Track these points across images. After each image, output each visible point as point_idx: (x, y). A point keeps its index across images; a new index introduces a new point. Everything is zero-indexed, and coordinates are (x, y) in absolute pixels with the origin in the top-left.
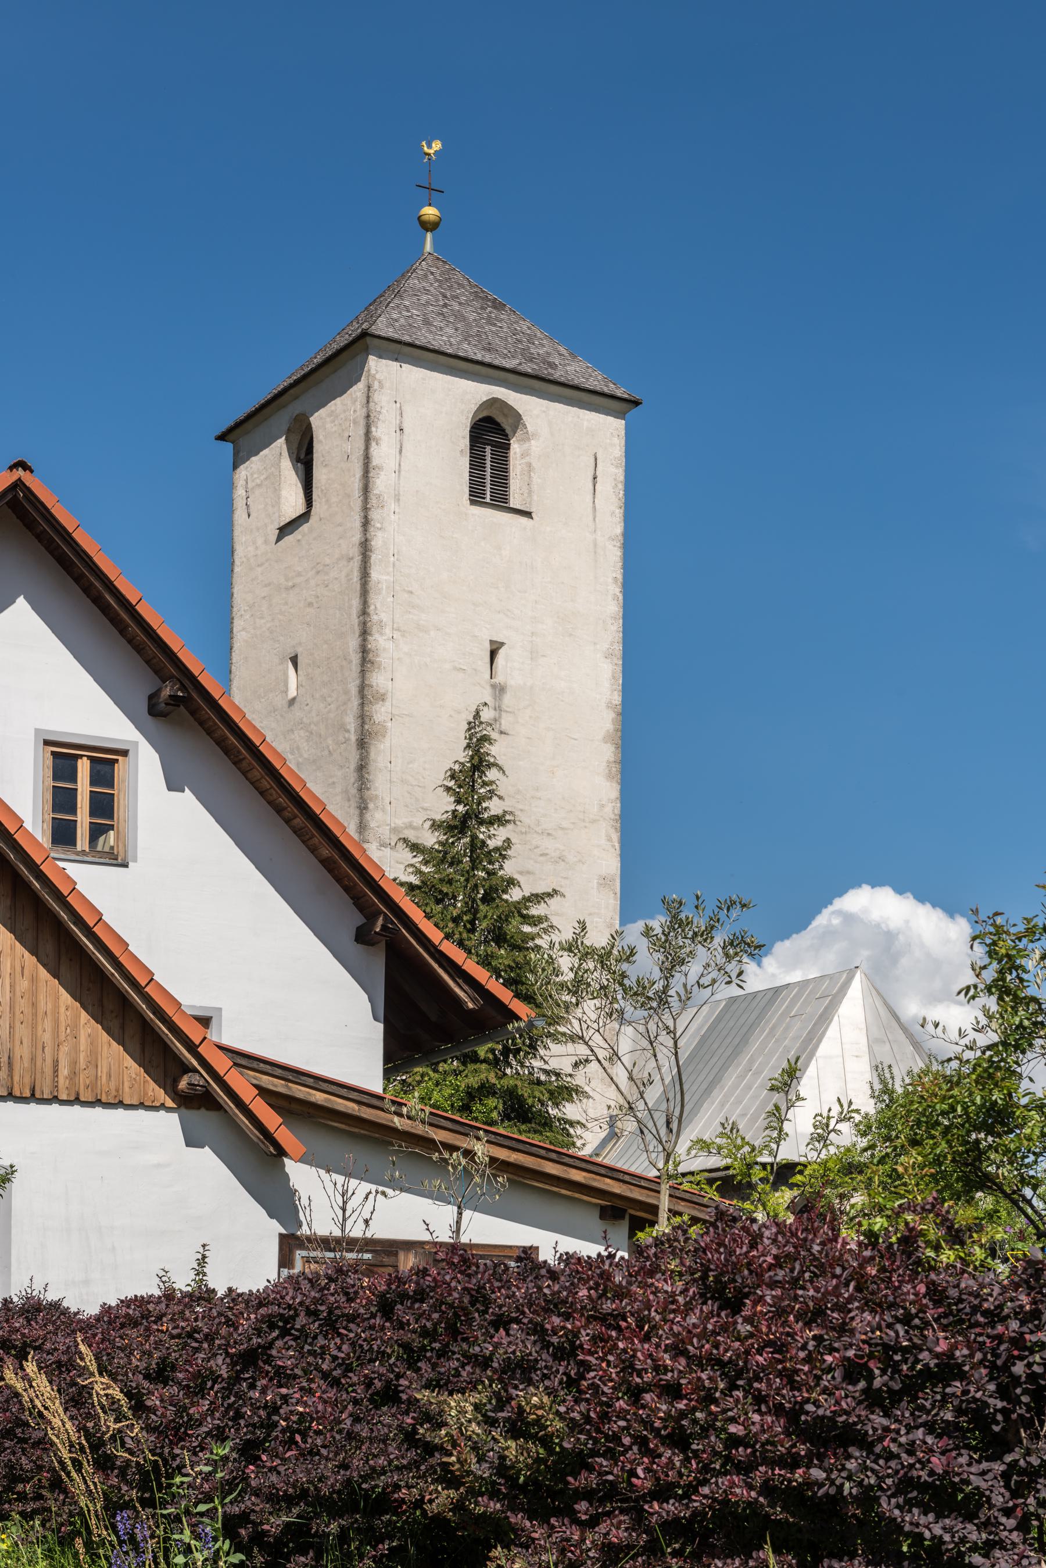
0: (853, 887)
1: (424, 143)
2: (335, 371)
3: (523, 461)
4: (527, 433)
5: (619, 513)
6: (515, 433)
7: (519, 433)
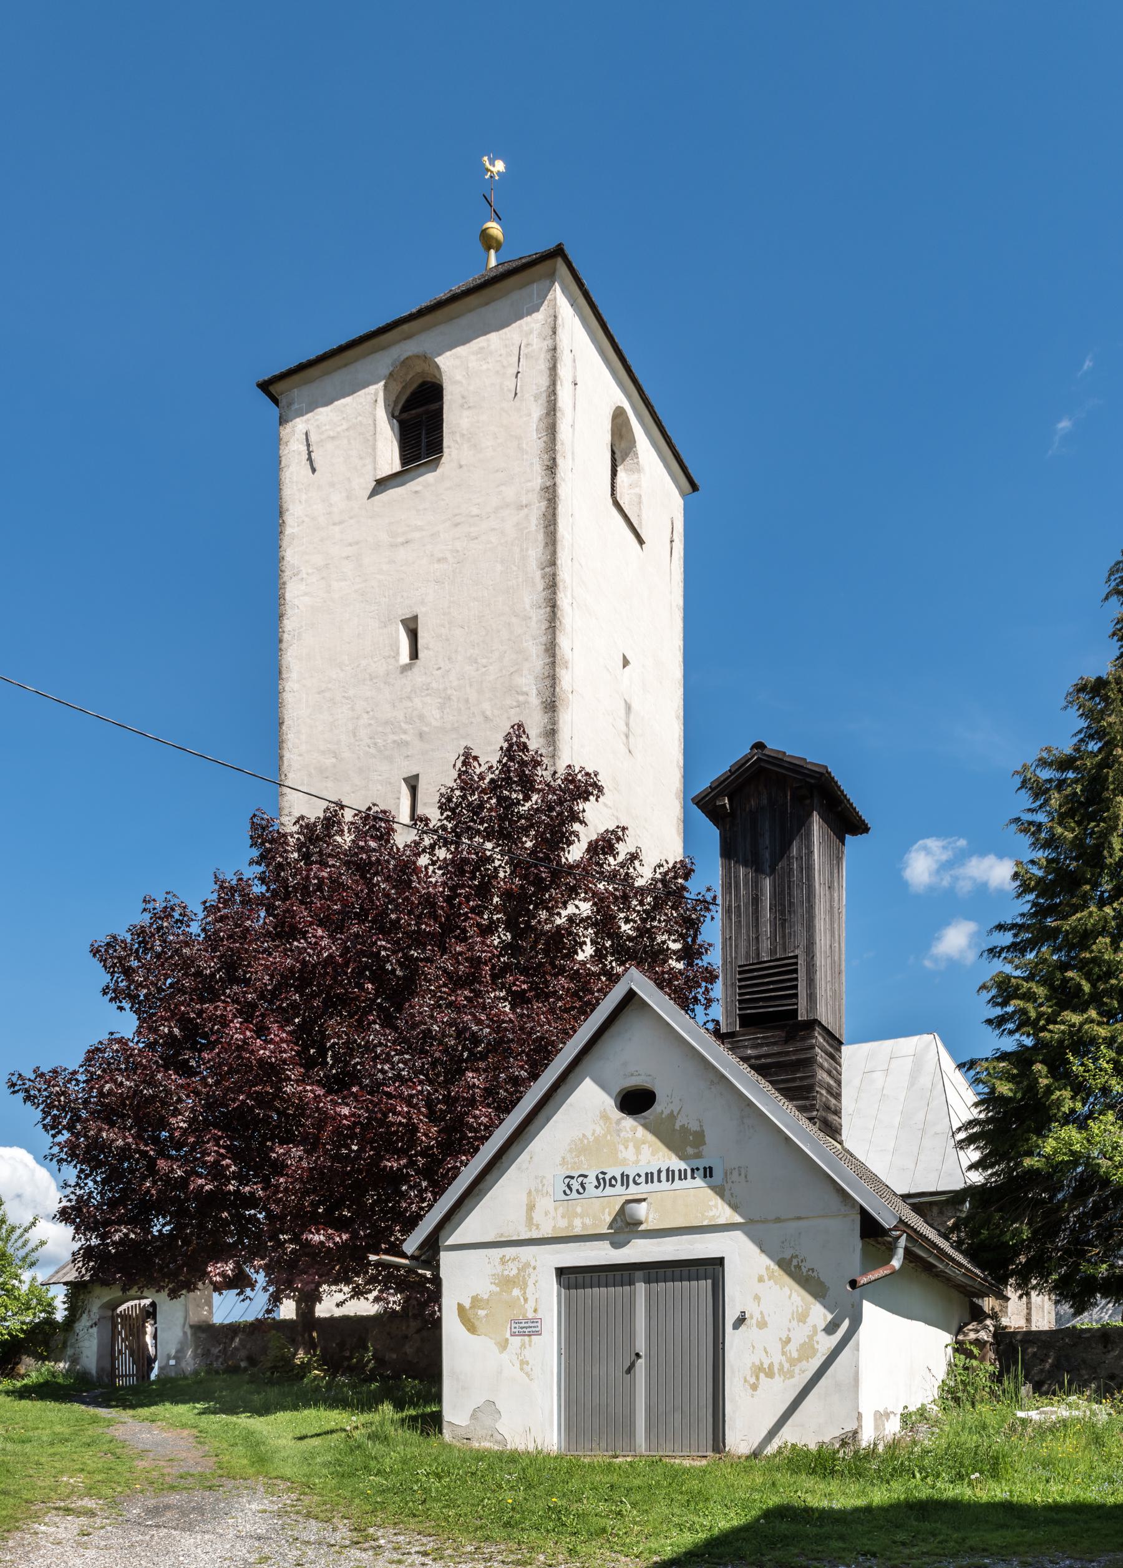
0: (26, 1149)
1: (486, 158)
2: (487, 304)
3: (633, 491)
4: (638, 463)
5: (681, 585)
6: (623, 460)
7: (628, 461)
